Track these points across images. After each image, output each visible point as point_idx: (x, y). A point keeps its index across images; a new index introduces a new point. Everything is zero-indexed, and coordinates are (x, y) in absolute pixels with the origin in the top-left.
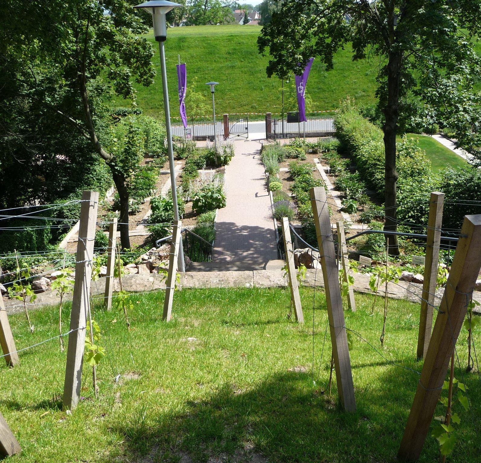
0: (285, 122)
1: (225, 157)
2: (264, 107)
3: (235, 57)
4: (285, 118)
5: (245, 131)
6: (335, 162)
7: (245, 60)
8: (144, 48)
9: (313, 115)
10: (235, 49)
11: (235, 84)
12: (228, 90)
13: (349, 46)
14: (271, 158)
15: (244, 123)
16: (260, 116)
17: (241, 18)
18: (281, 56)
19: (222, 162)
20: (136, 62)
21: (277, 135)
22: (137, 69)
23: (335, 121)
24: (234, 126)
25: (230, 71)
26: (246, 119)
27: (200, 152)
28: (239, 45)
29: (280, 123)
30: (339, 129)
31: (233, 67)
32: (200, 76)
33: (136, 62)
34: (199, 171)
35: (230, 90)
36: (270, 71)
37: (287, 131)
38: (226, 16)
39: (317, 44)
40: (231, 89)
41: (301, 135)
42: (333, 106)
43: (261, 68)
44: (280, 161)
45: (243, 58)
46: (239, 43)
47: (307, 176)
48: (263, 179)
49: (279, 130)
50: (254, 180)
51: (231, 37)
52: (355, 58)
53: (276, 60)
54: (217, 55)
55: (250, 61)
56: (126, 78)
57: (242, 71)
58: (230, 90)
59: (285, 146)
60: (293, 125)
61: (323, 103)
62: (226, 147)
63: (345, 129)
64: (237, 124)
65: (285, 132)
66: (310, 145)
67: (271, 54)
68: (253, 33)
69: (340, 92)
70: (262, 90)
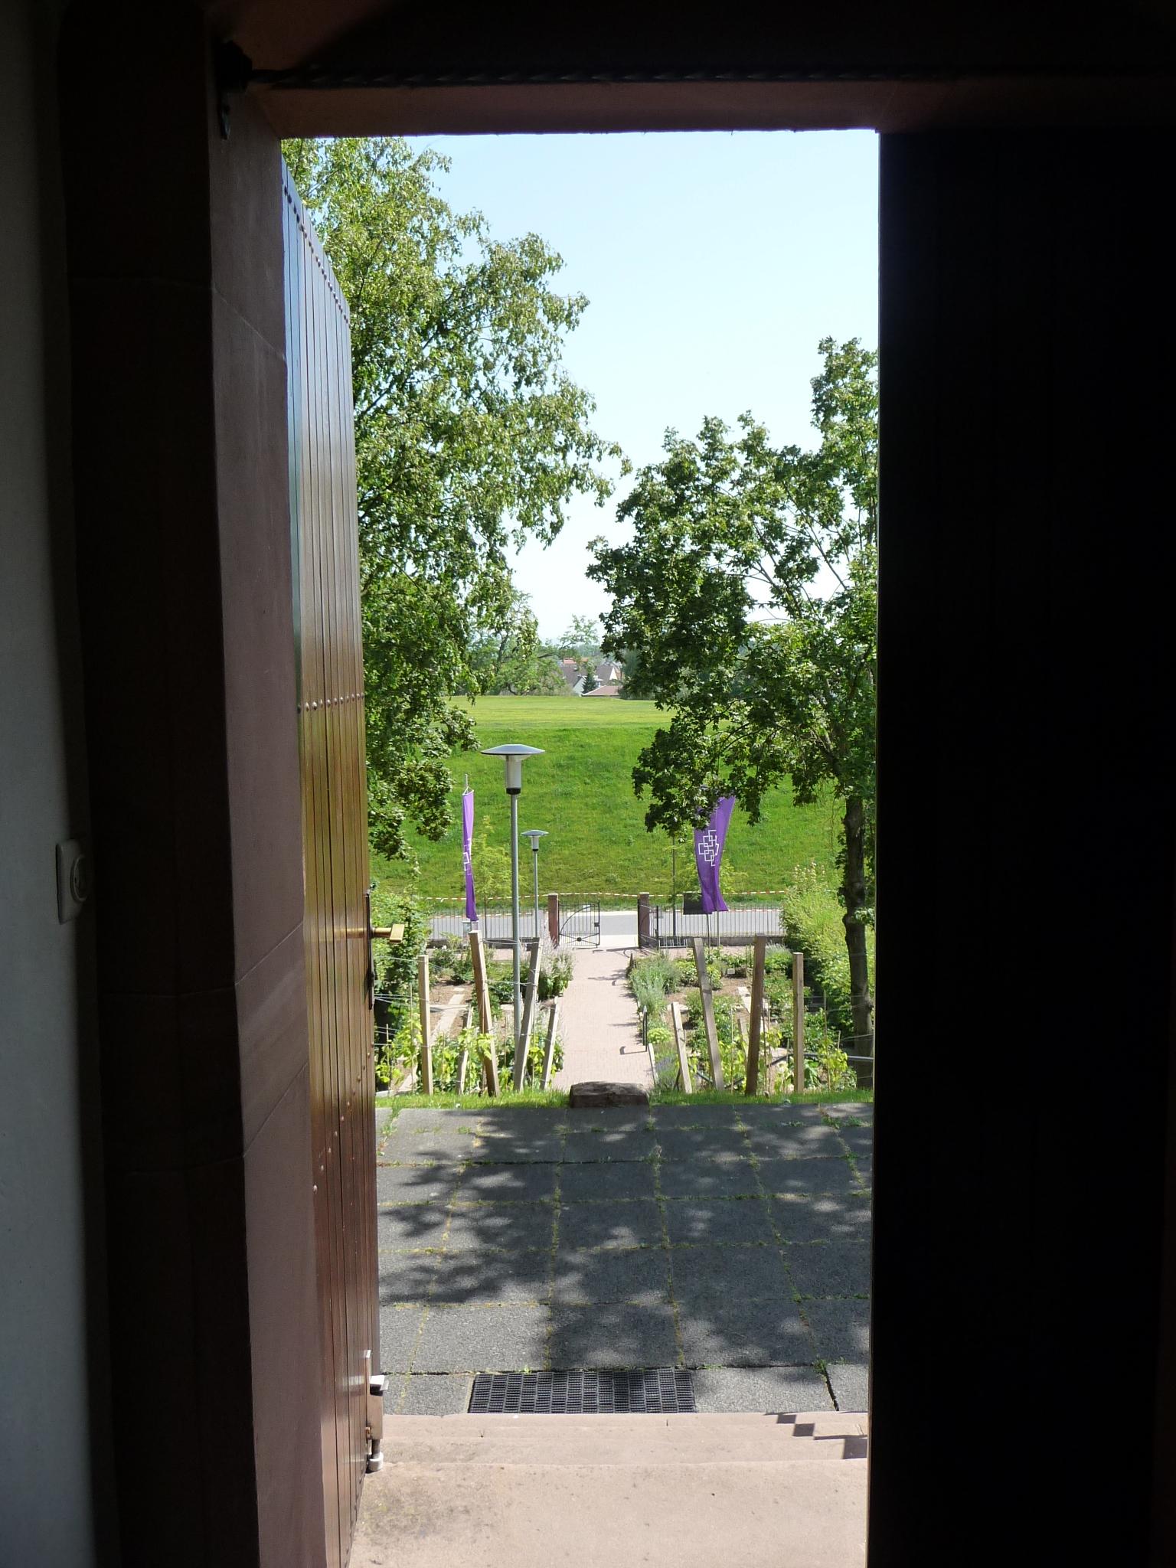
0: (679, 914)
1: (555, 979)
2: (634, 880)
3: (573, 774)
4: (679, 905)
5: (594, 929)
6: (780, 993)
7: (593, 781)
8: (438, 778)
9: (740, 899)
10: (571, 758)
11: (570, 831)
12: (556, 842)
13: (787, 783)
14: (649, 982)
15: (593, 913)
16: (624, 900)
17: (580, 678)
18: (671, 797)
19: (548, 990)
20: (420, 799)
21: (662, 940)
22: (420, 812)
23: (784, 912)
24: (566, 916)
25: (561, 803)
26: (597, 905)
27: (501, 970)
28: (580, 749)
29: (667, 914)
30: (792, 928)
31: (567, 795)
32: (496, 812)
33: (420, 799)
34: (503, 1007)
35: (561, 843)
36: (651, 821)
37: (684, 932)
38: (545, 675)
39: (732, 777)
40: (563, 842)
41: (711, 941)
42: (783, 881)
43: (627, 799)
44: (667, 990)
45: (590, 777)
46: (582, 746)
47: (723, 1017)
48: (634, 1024)
49: (666, 931)
50: (615, 1025)
51: (565, 733)
52: (799, 801)
53: (660, 803)
54: (534, 770)
55: (604, 784)
56: (394, 824)
57: (586, 805)
58: (561, 843)
59: (679, 960)
60: (692, 919)
61: (760, 875)
62: (557, 960)
63: (802, 927)
64: (577, 914)
65: (679, 934)
66: (731, 959)
67: (654, 795)
68: (611, 727)
69: (797, 853)
70: (629, 844)
